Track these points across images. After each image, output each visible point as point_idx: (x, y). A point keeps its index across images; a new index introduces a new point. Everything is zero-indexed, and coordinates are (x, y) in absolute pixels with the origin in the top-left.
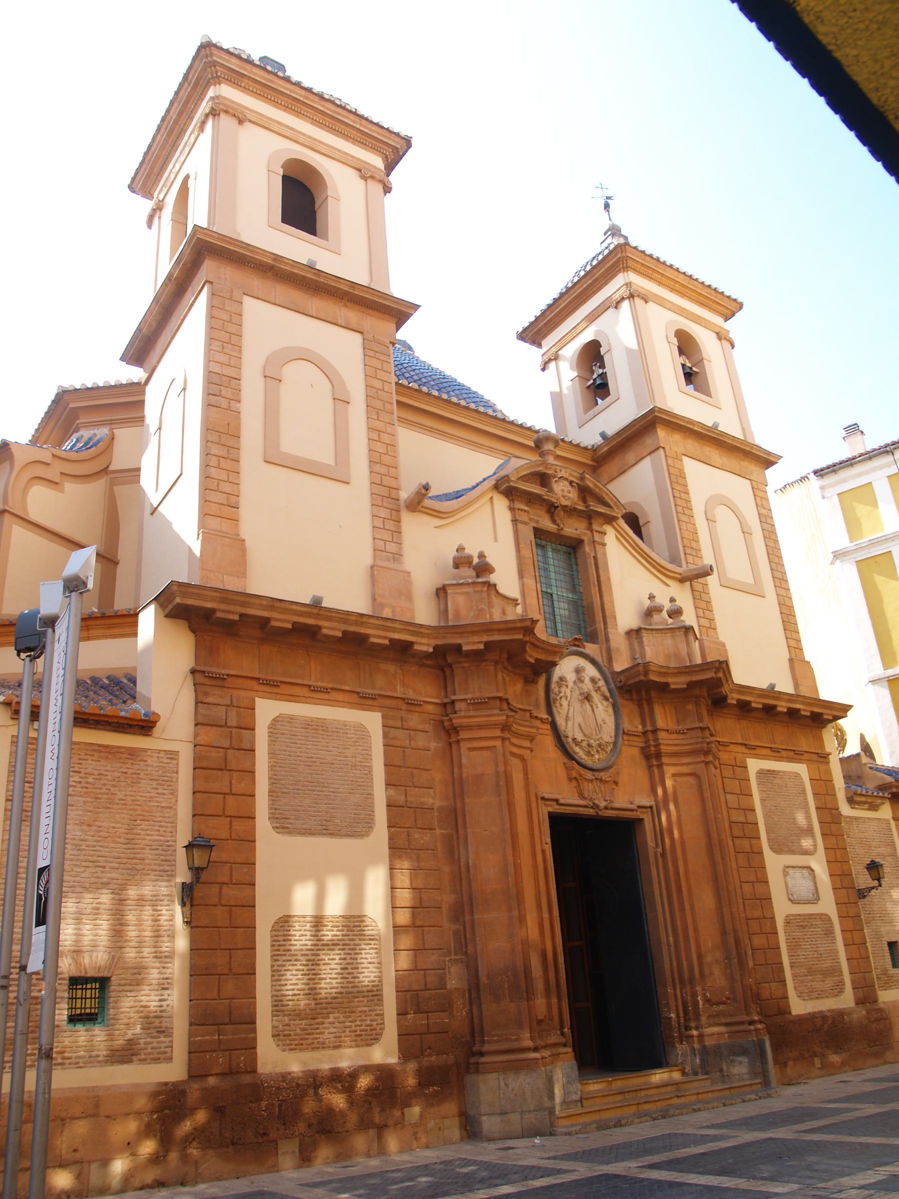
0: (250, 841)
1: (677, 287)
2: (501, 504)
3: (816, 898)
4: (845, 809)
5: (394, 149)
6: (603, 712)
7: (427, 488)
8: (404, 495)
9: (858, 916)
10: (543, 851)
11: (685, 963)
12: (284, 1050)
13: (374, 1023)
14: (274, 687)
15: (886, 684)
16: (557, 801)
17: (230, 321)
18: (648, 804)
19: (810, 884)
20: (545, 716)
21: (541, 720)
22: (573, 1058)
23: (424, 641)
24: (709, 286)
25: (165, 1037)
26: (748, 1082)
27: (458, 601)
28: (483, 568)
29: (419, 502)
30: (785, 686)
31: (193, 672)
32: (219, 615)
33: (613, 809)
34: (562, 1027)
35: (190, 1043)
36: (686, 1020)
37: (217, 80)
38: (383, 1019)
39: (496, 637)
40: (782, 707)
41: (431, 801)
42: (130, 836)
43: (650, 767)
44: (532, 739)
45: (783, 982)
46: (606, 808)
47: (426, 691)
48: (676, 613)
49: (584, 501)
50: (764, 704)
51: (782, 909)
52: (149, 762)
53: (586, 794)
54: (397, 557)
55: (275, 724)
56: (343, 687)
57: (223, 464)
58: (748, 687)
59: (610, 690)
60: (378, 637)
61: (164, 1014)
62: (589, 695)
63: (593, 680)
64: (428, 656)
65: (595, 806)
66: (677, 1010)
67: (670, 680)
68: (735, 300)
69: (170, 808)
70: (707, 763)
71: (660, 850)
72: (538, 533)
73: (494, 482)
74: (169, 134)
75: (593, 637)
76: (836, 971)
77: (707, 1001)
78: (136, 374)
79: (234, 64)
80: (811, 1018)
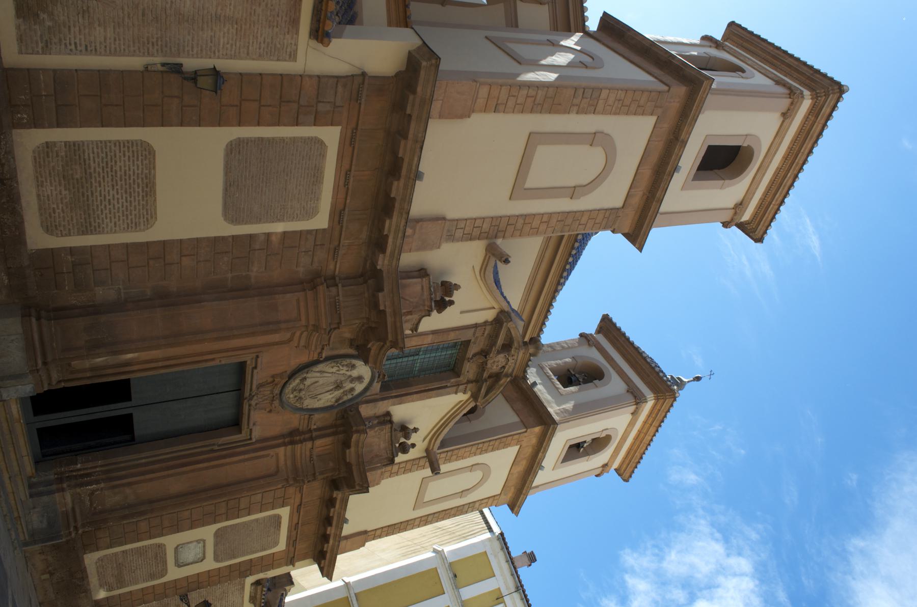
0: (220, 122)
1: (642, 435)
2: (490, 315)
3: (179, 565)
4: (250, 580)
5: (756, 230)
6: (327, 399)
7: (506, 261)
8: (499, 242)
9: (166, 597)
10: (213, 359)
11: (123, 473)
12: (34, 152)
13: (62, 228)
14: (349, 143)
15: (345, 595)
16: (255, 367)
17: (639, 106)
18: (253, 437)
19: (191, 559)
20: (324, 356)
21: (321, 353)
22: (39, 392)
23: (386, 262)
24: (641, 458)
25: (43, 48)
26: (25, 530)
27: (415, 287)
28: (442, 305)
29: (493, 255)
30: (347, 530)
31: (364, 74)
32: (411, 97)
33: (249, 410)
34: (64, 381)
35: (37, 70)
36: (75, 476)
37: (815, 97)
38: (66, 235)
39: (390, 320)
40: (331, 531)
41: (255, 269)
42: (222, 19)
43: (283, 436)
44: (307, 346)
45: (111, 546)
46: (250, 405)
47: (346, 262)
48: (404, 449)
49: (490, 377)
50: (332, 517)
51: (170, 541)
52: (287, 36)
53: (261, 389)
54: (451, 238)
55: (319, 143)
56: (349, 198)
57: (530, 100)
58: (346, 506)
59: (344, 402)
60: (391, 225)
61: (63, 46)
62: (341, 388)
63: (352, 389)
64: (374, 265)
65: (251, 397)
66: (84, 469)
67: (353, 449)
68: (631, 476)
69: (248, 54)
70: (287, 480)
71: (216, 448)
72: (467, 344)
73: (506, 309)
74: (774, 57)
75: (385, 387)
76: (121, 584)
77: (92, 493)
78: (593, 24)
79: (826, 110)
80: (84, 570)
